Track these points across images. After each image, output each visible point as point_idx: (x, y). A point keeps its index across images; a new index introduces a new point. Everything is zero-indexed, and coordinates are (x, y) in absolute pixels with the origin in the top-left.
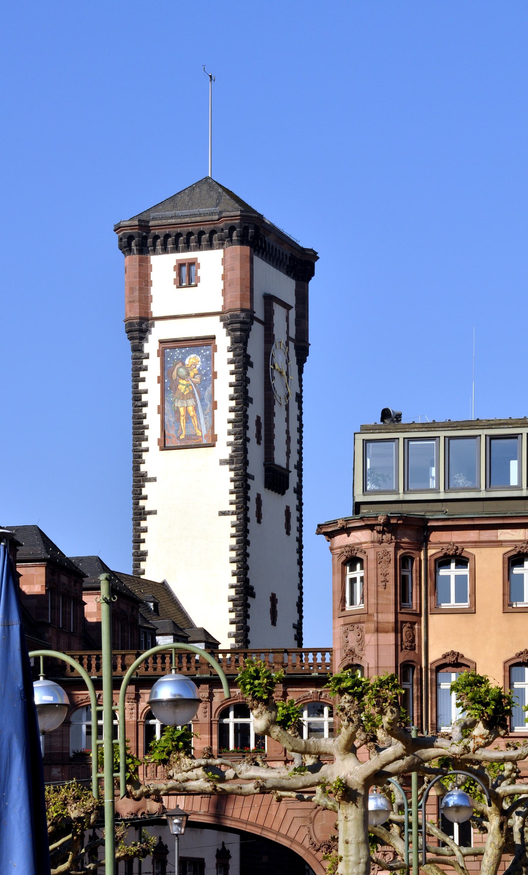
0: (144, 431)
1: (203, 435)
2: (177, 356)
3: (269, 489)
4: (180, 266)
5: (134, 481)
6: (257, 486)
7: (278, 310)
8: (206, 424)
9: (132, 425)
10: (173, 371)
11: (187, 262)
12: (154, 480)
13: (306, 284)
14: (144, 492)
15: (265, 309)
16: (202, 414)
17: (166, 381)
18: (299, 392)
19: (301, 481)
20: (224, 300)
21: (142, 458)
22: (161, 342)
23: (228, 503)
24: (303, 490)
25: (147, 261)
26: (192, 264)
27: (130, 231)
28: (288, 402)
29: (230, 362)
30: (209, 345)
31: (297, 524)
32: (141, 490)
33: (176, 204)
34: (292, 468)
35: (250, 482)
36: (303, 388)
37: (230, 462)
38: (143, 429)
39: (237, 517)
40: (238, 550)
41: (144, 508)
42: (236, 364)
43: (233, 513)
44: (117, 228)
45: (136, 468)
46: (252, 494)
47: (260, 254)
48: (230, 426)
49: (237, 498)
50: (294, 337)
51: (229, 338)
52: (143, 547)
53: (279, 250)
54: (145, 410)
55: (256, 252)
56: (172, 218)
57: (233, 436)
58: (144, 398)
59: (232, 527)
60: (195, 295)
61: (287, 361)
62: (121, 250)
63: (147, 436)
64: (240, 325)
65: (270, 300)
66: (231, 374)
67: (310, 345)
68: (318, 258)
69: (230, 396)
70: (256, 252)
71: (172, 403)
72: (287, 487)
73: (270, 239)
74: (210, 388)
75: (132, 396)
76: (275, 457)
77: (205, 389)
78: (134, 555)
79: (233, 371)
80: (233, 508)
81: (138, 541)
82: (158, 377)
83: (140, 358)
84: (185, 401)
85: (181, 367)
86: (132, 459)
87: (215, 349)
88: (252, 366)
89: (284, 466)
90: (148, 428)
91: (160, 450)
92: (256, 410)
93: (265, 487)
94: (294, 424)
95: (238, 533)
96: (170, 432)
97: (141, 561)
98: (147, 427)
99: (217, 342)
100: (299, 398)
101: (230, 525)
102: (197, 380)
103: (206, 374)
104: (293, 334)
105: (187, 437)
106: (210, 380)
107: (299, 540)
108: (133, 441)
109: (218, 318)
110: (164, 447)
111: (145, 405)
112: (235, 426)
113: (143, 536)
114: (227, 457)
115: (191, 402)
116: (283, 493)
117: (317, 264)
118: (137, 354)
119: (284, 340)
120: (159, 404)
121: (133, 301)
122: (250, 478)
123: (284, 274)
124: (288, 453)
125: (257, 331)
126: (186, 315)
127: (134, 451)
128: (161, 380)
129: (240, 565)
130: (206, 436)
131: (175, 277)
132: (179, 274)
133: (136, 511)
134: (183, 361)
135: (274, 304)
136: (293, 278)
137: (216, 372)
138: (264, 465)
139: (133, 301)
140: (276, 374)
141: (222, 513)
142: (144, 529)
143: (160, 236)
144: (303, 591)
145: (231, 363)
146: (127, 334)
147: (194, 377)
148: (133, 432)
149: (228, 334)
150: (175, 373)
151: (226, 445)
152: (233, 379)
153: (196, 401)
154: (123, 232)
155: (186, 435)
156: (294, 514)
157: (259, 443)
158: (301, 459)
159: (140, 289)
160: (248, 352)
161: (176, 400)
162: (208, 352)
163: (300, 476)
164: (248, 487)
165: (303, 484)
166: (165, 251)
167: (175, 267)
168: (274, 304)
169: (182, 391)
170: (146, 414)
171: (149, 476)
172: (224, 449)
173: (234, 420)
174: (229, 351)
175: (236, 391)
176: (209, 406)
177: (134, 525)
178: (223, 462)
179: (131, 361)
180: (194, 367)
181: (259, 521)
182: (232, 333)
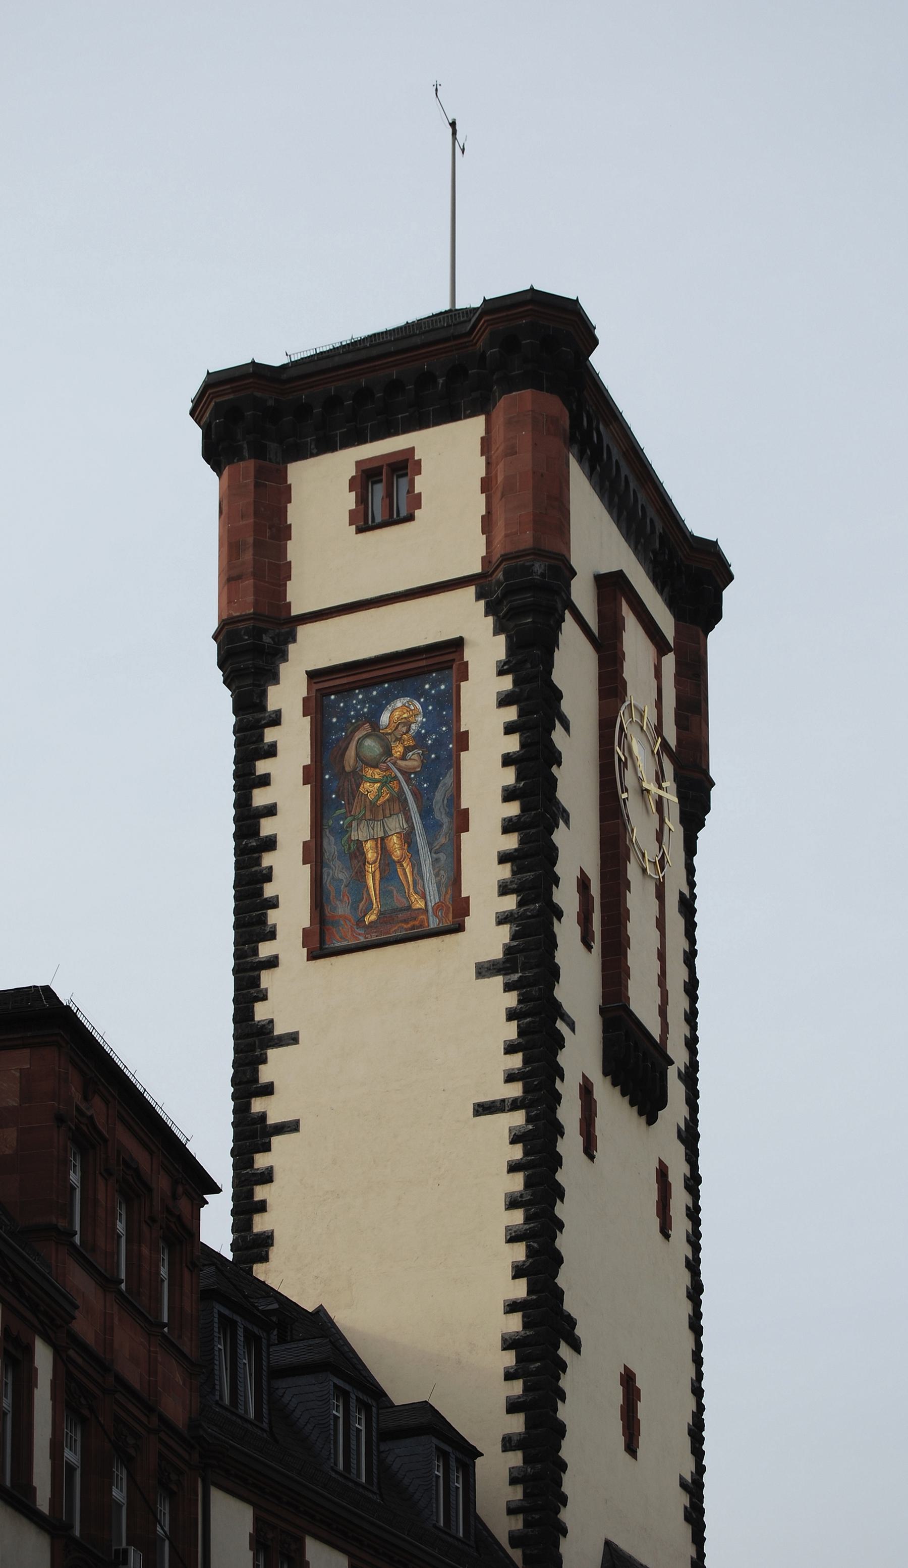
2: (355, 709)
4: (367, 477)
6: (581, 1054)
8: (437, 875)
10: (346, 748)
12: (292, 1039)
14: (266, 1074)
16: (427, 849)
18: (686, 891)
21: (259, 986)
22: (313, 676)
23: (501, 1077)
26: (404, 466)
28: (663, 877)
29: (504, 701)
31: (688, 1225)
32: (256, 1071)
39: (527, 1113)
43: (514, 1105)
48: (505, 872)
51: (502, 639)
52: (261, 1224)
54: (268, 860)
70: (575, 449)
74: (448, 780)
77: (434, 785)
96: (341, 909)
98: (274, 903)
99: (469, 655)
100: (688, 907)
102: (413, 761)
103: (439, 744)
109: (470, 591)
110: (319, 946)
113: (261, 1193)
114: (497, 953)
115: (396, 824)
117: (729, 594)
130: (438, 907)
132: (362, 500)
134: (373, 719)
137: (466, 733)
138: (602, 1011)
141: (483, 1109)
147: (403, 758)
150: (351, 753)
153: (408, 819)
154: (213, 404)
155: (381, 914)
159: (258, 545)
161: (354, 824)
162: (443, 687)
167: (352, 481)
169: (371, 797)
171: (279, 1030)
178: (484, 970)
180: (404, 729)
181: (589, 1149)
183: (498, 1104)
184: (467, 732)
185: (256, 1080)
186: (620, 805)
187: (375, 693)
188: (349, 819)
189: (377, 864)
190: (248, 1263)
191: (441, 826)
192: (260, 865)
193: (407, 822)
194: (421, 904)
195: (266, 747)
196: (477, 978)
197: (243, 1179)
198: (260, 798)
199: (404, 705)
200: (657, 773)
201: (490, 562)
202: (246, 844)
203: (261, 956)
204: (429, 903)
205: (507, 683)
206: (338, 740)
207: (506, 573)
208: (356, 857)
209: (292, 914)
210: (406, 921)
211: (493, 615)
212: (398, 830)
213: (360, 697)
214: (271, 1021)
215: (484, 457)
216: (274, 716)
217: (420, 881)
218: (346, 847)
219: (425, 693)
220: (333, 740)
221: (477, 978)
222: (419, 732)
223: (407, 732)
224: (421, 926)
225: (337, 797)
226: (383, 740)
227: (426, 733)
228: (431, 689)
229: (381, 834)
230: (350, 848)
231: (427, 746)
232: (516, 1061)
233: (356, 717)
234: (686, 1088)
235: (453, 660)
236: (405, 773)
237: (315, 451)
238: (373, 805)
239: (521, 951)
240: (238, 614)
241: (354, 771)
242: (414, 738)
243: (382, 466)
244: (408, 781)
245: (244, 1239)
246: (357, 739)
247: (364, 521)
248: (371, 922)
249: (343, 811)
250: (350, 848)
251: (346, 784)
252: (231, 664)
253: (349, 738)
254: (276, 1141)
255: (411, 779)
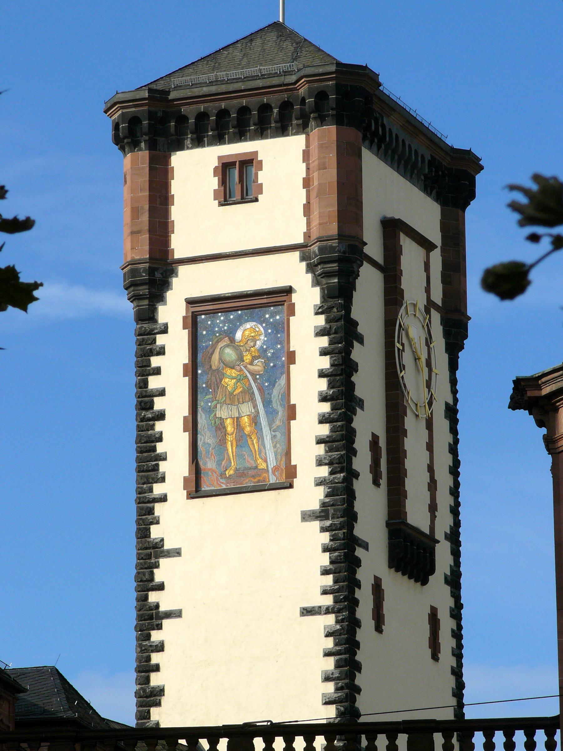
0: (157, 465)
1: (270, 467)
2: (219, 327)
3: (397, 571)
4: (225, 168)
5: (139, 557)
6: (374, 561)
7: (408, 247)
8: (275, 447)
9: (134, 455)
10: (212, 354)
11: (237, 160)
12: (177, 553)
13: (460, 212)
14: (159, 576)
15: (384, 255)
16: (268, 428)
17: (199, 372)
18: (451, 402)
19: (457, 563)
20: (309, 224)
21: (153, 514)
22: (190, 302)
23: (319, 591)
24: (462, 581)
25: (166, 161)
26: (248, 163)
27: (133, 109)
28: (432, 413)
29: (321, 333)
30: (281, 303)
31: (453, 643)
32: (152, 574)
33: (219, 64)
34: (439, 535)
35: (359, 552)
36: (458, 396)
37: (322, 514)
38: (156, 460)
39: (336, 617)
40: (338, 679)
41: (157, 606)
42: (332, 336)
43: (328, 611)
44: (109, 105)
45: (143, 533)
46: (365, 575)
47: (375, 147)
48: (321, 450)
49: (336, 581)
50: (440, 303)
51: (317, 290)
52: (155, 680)
53: (410, 146)
54: (159, 426)
55: (367, 143)
56: (211, 83)
57: (327, 467)
58: (159, 404)
59: (327, 636)
60: (251, 219)
61: (429, 341)
62: (117, 145)
63: (164, 473)
64: (337, 263)
65: (392, 228)
66: (321, 355)
67: (469, 318)
68: (482, 168)
69: (320, 393)
70: (367, 143)
71: (210, 411)
72: (432, 571)
73: (392, 123)
74: (282, 381)
75: (135, 403)
76: (407, 509)
77: (273, 384)
78: (137, 694)
79: (325, 348)
80: (328, 600)
81: (146, 669)
82: (185, 365)
83: (152, 333)
84: (234, 408)
85: (227, 346)
86: (134, 516)
87: (292, 311)
88: (361, 342)
89: (427, 531)
90: (165, 459)
91: (188, 498)
92: (369, 422)
93: (390, 567)
94: (443, 460)
95: (338, 648)
96: (208, 464)
97: (151, 706)
98: (163, 457)
99: (295, 298)
100: (451, 412)
101: (322, 633)
102: (258, 366)
103: (276, 356)
104: (437, 296)
105: (241, 473)
106: (283, 366)
107: (457, 672)
108: (138, 482)
109: (296, 255)
110: (196, 488)
111: (161, 416)
112: (330, 450)
113: (156, 658)
114: (315, 506)
115: (246, 409)
116: (424, 582)
117: (480, 178)
118: (145, 326)
119: (422, 302)
120: (186, 361)
121: (139, 232)
122: (360, 546)
123: (420, 189)
124: (433, 508)
125: (369, 285)
126: (236, 252)
127: (140, 501)
128: (192, 370)
129: (342, 709)
130: (275, 469)
131: (217, 187)
132: (223, 182)
133: (141, 612)
134: (230, 334)
135: (402, 236)
136: (437, 199)
137: (294, 352)
138: (388, 525)
139: (139, 232)
140: (407, 358)
141: (307, 612)
142: (156, 646)
143: (189, 116)
144: (460, 500)
145: (323, 335)
146: (126, 292)
147: (251, 363)
148: (138, 467)
149: (316, 283)
150: (216, 357)
151: (314, 442)
152: (325, 363)
153: (255, 406)
154: (120, 112)
155: (236, 470)
156: (447, 624)
157: (376, 482)
158: (457, 524)
159: (152, 210)
160: (354, 315)
161: (218, 406)
162: (278, 317)
163: (456, 553)
164: (357, 562)
165: (463, 569)
166: (199, 142)
167: (216, 169)
168: (402, 236)
169: (229, 388)
170: (159, 517)
171: (167, 546)
172: (309, 491)
173: (328, 437)
174: (317, 313)
175: (331, 385)
176: (281, 413)
177: (138, 639)
178: (307, 516)
179: (135, 339)
180: (252, 344)
181: (379, 629)
182: (324, 281)
183: (317, 610)
184: (294, 352)
185: (152, 579)
186: (399, 381)
187: (232, 317)
188: (215, 402)
189: (234, 435)
190: (147, 707)
191: (277, 413)
192: (154, 430)
193: (254, 408)
194: (263, 466)
195: (158, 349)
196: (302, 521)
197: (143, 648)
198: (154, 383)
199: (252, 327)
200: (426, 339)
201: (310, 237)
202: (145, 416)
203: (156, 430)
204: (269, 466)
205: (321, 320)
206: (207, 347)
207: (321, 249)
208: (220, 429)
209: (175, 464)
210: (253, 477)
211: (312, 273)
212: (248, 413)
213: (222, 318)
214: (162, 540)
215: (305, 164)
216: (163, 327)
217: (263, 450)
218: (213, 422)
219: (266, 321)
220: (203, 346)
221: (302, 521)
222: (262, 347)
223: (254, 346)
224: (264, 481)
225: (207, 386)
226: (237, 350)
227: (267, 348)
228: (270, 318)
229: (237, 415)
230: (215, 422)
231: (267, 358)
232: (329, 580)
233: (219, 332)
234: (451, 543)
235: (285, 301)
236: (253, 374)
237: (190, 146)
238: (231, 394)
239: (333, 505)
240: (138, 258)
241: (218, 370)
242: (258, 351)
243: (236, 162)
244: (255, 380)
245: (144, 690)
246: (220, 347)
247: (226, 197)
248: (230, 475)
249: (211, 396)
250: (215, 422)
251: (213, 378)
252: (133, 291)
253: (214, 347)
254: (166, 623)
255: (257, 379)
